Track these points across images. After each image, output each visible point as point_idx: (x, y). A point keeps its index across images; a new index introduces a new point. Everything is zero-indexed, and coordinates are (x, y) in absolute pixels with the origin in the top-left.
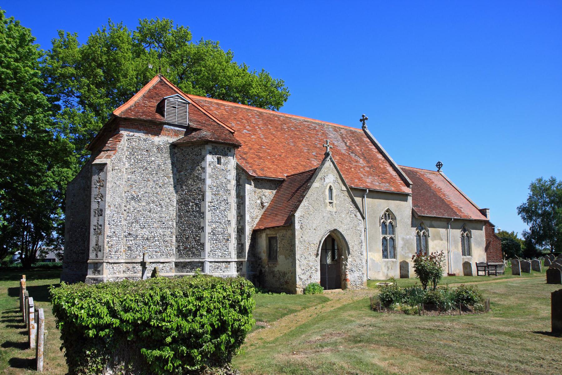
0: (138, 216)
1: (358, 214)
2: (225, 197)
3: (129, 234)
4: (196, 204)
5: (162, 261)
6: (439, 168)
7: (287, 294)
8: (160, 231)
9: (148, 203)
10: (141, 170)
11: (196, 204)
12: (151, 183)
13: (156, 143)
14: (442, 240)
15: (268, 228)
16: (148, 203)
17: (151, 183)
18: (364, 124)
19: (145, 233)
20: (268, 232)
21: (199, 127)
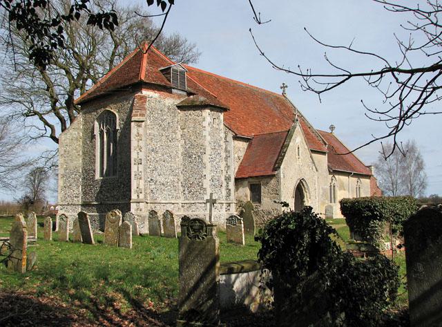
0: (157, 165)
1: (314, 168)
2: (219, 151)
3: (151, 180)
4: (199, 156)
5: (173, 202)
6: (332, 130)
7: (342, 214)
8: (171, 178)
9: (163, 155)
10: (157, 126)
11: (199, 156)
12: (164, 138)
13: (167, 104)
14: (345, 190)
15: (251, 177)
16: (163, 155)
17: (164, 138)
18: (284, 91)
19: (161, 179)
20: (251, 180)
21: (195, 92)
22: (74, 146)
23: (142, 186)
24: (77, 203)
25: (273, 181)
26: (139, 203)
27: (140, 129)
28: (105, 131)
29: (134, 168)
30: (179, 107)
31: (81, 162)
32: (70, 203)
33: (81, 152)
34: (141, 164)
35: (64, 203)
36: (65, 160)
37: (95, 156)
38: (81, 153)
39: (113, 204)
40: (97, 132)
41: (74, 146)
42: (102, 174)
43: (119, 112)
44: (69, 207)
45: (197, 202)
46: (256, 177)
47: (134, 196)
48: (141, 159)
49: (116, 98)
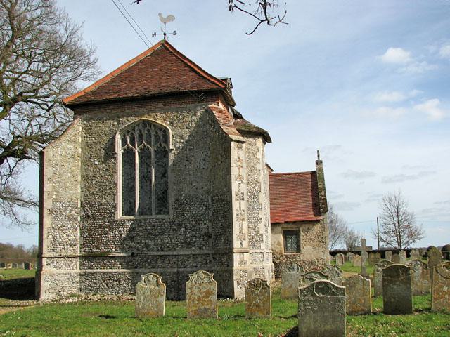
15: (286, 222)
20: (285, 226)
22: (68, 166)
23: (245, 231)
24: (74, 255)
25: (317, 227)
26: (243, 253)
27: (240, 152)
28: (137, 150)
29: (236, 205)
30: (266, 138)
31: (79, 191)
32: (63, 255)
33: (80, 177)
34: (243, 199)
35: (52, 255)
36: (54, 187)
37: (115, 184)
38: (79, 178)
39: (161, 256)
40: (119, 149)
41: (68, 166)
42: (129, 211)
43: (172, 124)
44: (61, 261)
45: (254, 251)
46: (295, 222)
47: (236, 245)
48: (242, 194)
49: (161, 105)
